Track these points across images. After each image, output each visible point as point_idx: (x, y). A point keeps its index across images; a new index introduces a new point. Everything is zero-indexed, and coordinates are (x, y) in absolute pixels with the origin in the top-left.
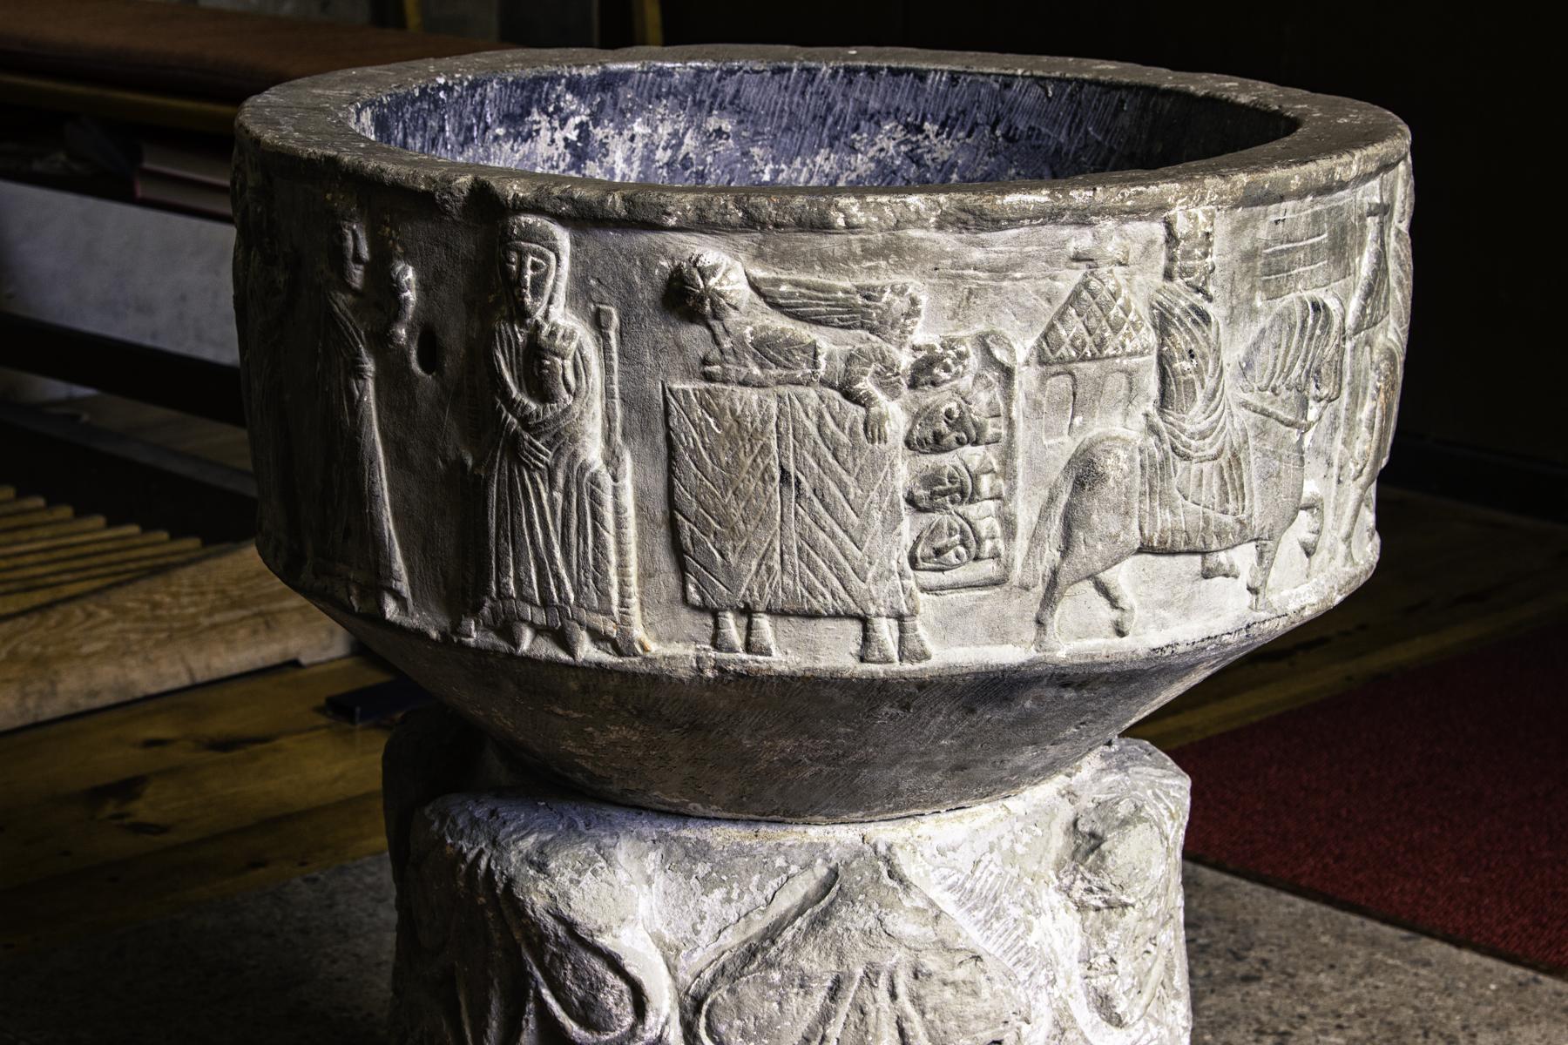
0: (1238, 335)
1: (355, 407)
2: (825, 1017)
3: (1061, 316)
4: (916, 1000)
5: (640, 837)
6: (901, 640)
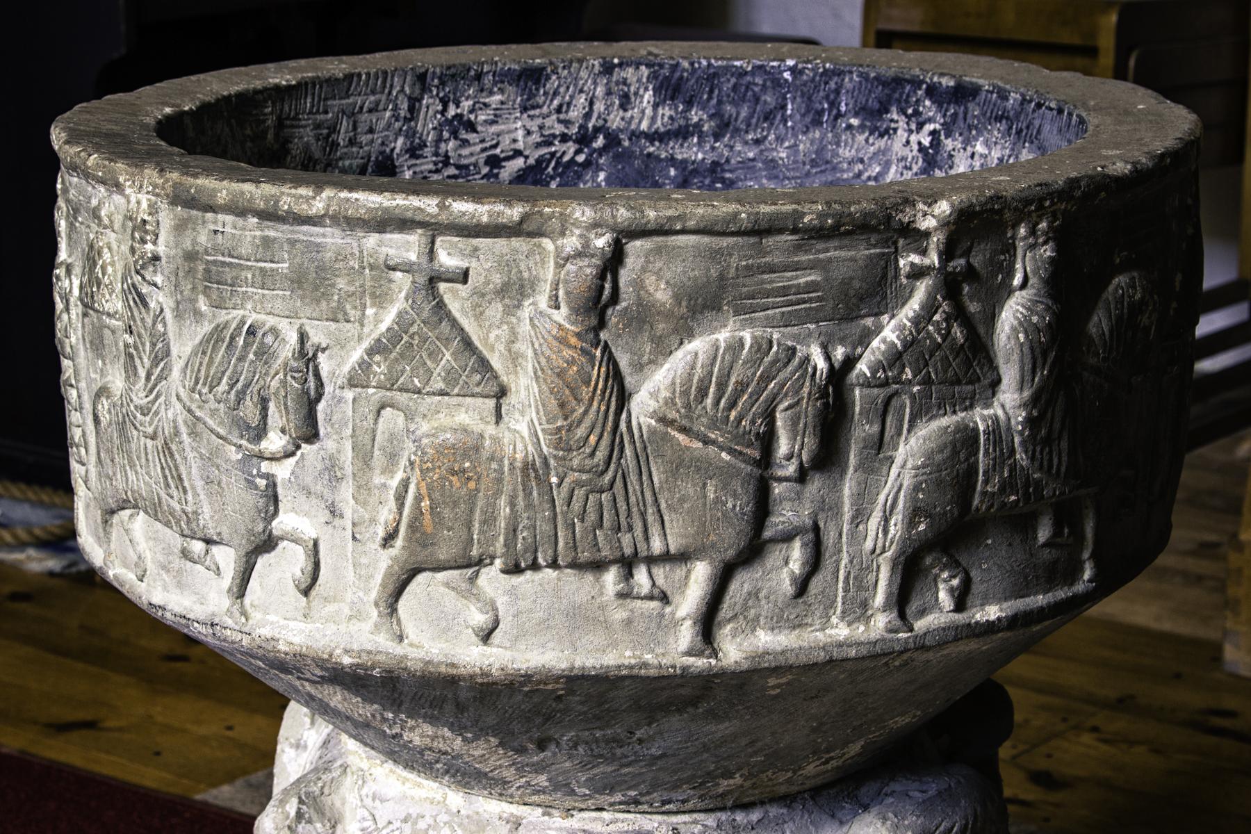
0: (185, 331)
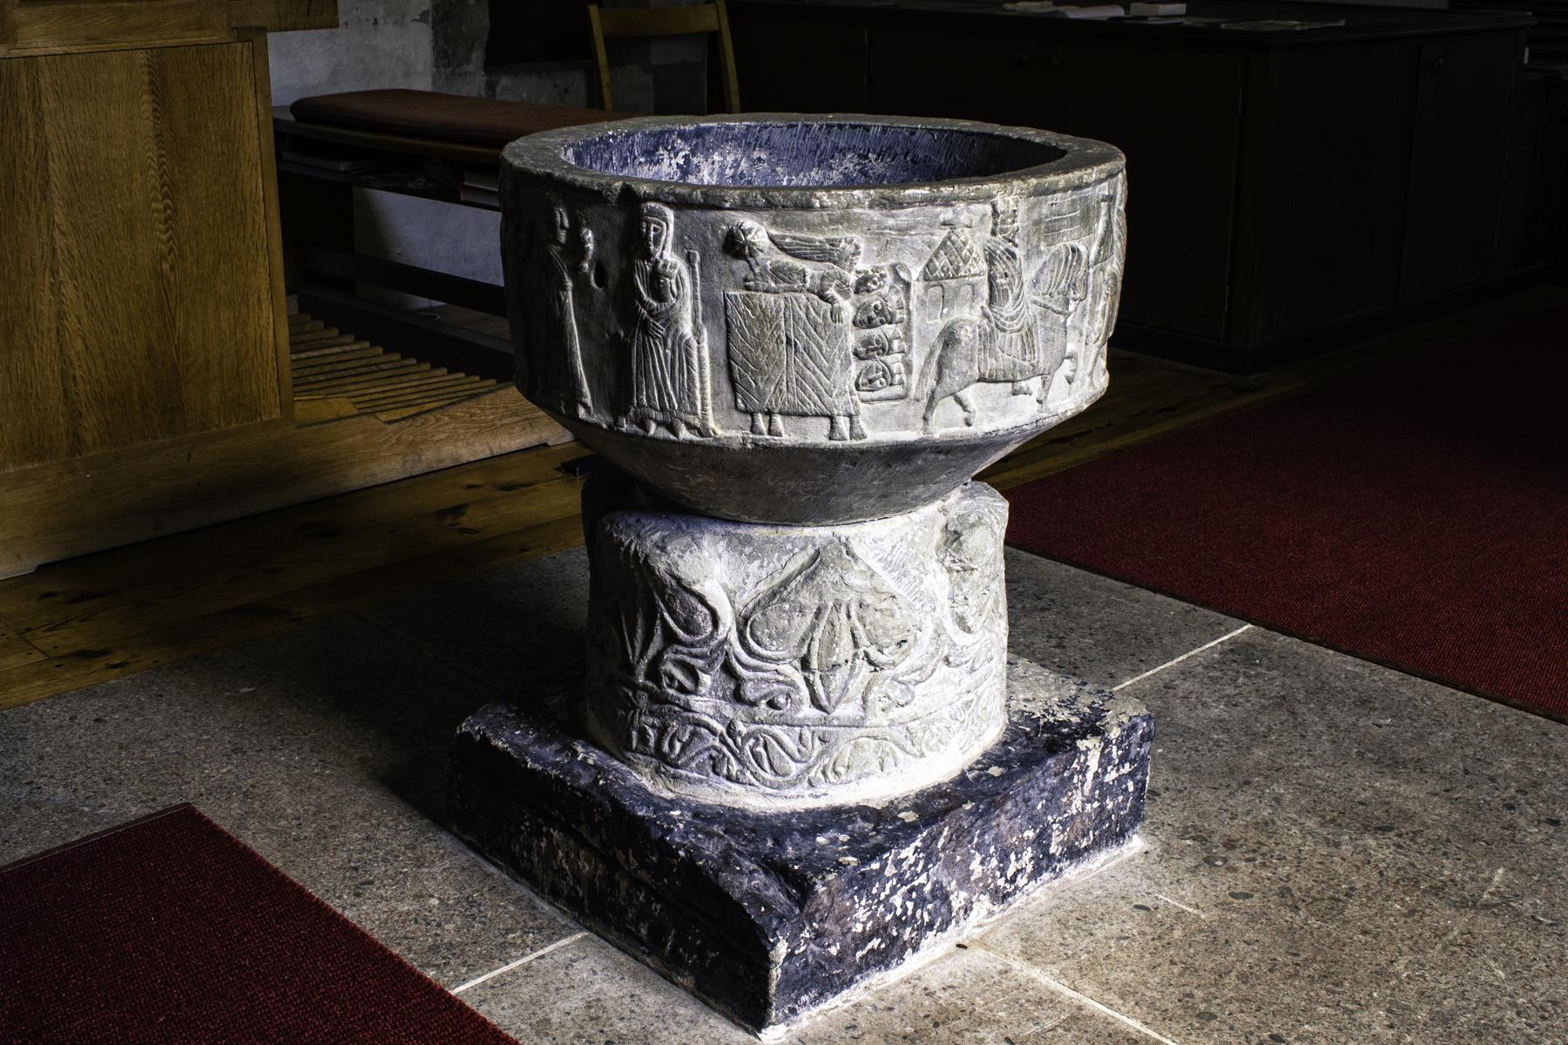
1: (562, 305)
2: (813, 628)
3: (936, 255)
4: (861, 619)
5: (715, 533)
6: (851, 429)
